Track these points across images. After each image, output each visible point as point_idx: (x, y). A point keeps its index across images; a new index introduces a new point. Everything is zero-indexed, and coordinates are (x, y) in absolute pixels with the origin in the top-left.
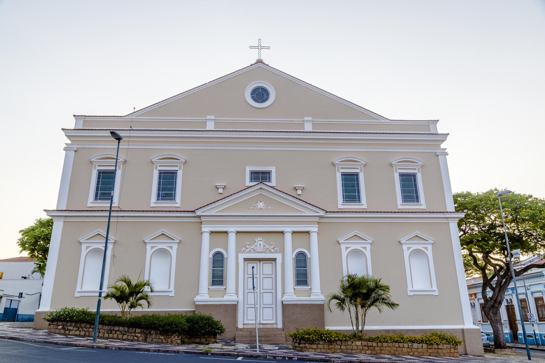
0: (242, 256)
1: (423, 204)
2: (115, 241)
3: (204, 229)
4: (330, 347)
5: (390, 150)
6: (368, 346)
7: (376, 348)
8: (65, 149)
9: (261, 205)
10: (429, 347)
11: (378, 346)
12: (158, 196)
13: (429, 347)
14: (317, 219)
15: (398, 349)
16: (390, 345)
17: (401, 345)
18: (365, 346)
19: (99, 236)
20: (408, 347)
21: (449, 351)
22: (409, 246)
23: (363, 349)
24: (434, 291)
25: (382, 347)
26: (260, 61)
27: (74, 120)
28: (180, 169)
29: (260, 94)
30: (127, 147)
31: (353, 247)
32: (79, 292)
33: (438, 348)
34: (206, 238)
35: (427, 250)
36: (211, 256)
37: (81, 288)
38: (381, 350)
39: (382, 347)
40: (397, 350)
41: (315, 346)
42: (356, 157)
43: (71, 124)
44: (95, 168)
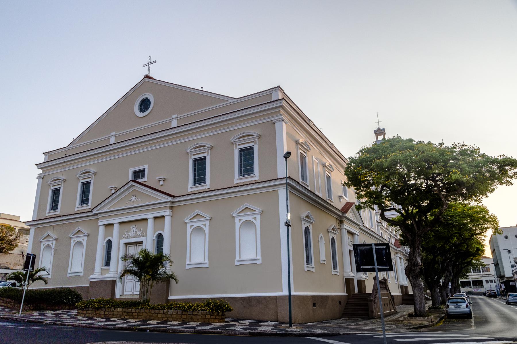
0: (123, 241)
1: (257, 176)
2: (261, 211)
3: (100, 224)
4: (97, 312)
5: (82, 165)
6: (127, 312)
7: (134, 314)
8: (38, 178)
9: (133, 198)
10: (184, 313)
11: (135, 312)
12: (241, 172)
13: (184, 313)
14: (169, 205)
15: (154, 315)
16: (147, 311)
17: (157, 311)
18: (124, 312)
19: (247, 209)
20: (164, 314)
21: (204, 317)
22: (241, 218)
23: (123, 315)
24: (258, 260)
25: (139, 313)
26: (147, 77)
27: (43, 156)
28: (208, 154)
29: (145, 105)
30: (62, 170)
31: (245, 219)
32: (238, 261)
33: (193, 315)
34: (102, 229)
35: (205, 226)
36: (154, 238)
37: (190, 262)
38: (138, 315)
39: (139, 313)
40: (152, 316)
41: (85, 312)
42: (203, 143)
43: (42, 159)
44: (236, 147)
